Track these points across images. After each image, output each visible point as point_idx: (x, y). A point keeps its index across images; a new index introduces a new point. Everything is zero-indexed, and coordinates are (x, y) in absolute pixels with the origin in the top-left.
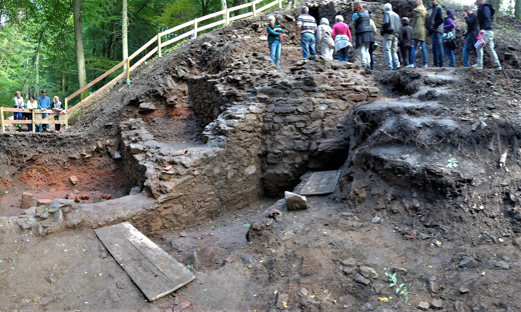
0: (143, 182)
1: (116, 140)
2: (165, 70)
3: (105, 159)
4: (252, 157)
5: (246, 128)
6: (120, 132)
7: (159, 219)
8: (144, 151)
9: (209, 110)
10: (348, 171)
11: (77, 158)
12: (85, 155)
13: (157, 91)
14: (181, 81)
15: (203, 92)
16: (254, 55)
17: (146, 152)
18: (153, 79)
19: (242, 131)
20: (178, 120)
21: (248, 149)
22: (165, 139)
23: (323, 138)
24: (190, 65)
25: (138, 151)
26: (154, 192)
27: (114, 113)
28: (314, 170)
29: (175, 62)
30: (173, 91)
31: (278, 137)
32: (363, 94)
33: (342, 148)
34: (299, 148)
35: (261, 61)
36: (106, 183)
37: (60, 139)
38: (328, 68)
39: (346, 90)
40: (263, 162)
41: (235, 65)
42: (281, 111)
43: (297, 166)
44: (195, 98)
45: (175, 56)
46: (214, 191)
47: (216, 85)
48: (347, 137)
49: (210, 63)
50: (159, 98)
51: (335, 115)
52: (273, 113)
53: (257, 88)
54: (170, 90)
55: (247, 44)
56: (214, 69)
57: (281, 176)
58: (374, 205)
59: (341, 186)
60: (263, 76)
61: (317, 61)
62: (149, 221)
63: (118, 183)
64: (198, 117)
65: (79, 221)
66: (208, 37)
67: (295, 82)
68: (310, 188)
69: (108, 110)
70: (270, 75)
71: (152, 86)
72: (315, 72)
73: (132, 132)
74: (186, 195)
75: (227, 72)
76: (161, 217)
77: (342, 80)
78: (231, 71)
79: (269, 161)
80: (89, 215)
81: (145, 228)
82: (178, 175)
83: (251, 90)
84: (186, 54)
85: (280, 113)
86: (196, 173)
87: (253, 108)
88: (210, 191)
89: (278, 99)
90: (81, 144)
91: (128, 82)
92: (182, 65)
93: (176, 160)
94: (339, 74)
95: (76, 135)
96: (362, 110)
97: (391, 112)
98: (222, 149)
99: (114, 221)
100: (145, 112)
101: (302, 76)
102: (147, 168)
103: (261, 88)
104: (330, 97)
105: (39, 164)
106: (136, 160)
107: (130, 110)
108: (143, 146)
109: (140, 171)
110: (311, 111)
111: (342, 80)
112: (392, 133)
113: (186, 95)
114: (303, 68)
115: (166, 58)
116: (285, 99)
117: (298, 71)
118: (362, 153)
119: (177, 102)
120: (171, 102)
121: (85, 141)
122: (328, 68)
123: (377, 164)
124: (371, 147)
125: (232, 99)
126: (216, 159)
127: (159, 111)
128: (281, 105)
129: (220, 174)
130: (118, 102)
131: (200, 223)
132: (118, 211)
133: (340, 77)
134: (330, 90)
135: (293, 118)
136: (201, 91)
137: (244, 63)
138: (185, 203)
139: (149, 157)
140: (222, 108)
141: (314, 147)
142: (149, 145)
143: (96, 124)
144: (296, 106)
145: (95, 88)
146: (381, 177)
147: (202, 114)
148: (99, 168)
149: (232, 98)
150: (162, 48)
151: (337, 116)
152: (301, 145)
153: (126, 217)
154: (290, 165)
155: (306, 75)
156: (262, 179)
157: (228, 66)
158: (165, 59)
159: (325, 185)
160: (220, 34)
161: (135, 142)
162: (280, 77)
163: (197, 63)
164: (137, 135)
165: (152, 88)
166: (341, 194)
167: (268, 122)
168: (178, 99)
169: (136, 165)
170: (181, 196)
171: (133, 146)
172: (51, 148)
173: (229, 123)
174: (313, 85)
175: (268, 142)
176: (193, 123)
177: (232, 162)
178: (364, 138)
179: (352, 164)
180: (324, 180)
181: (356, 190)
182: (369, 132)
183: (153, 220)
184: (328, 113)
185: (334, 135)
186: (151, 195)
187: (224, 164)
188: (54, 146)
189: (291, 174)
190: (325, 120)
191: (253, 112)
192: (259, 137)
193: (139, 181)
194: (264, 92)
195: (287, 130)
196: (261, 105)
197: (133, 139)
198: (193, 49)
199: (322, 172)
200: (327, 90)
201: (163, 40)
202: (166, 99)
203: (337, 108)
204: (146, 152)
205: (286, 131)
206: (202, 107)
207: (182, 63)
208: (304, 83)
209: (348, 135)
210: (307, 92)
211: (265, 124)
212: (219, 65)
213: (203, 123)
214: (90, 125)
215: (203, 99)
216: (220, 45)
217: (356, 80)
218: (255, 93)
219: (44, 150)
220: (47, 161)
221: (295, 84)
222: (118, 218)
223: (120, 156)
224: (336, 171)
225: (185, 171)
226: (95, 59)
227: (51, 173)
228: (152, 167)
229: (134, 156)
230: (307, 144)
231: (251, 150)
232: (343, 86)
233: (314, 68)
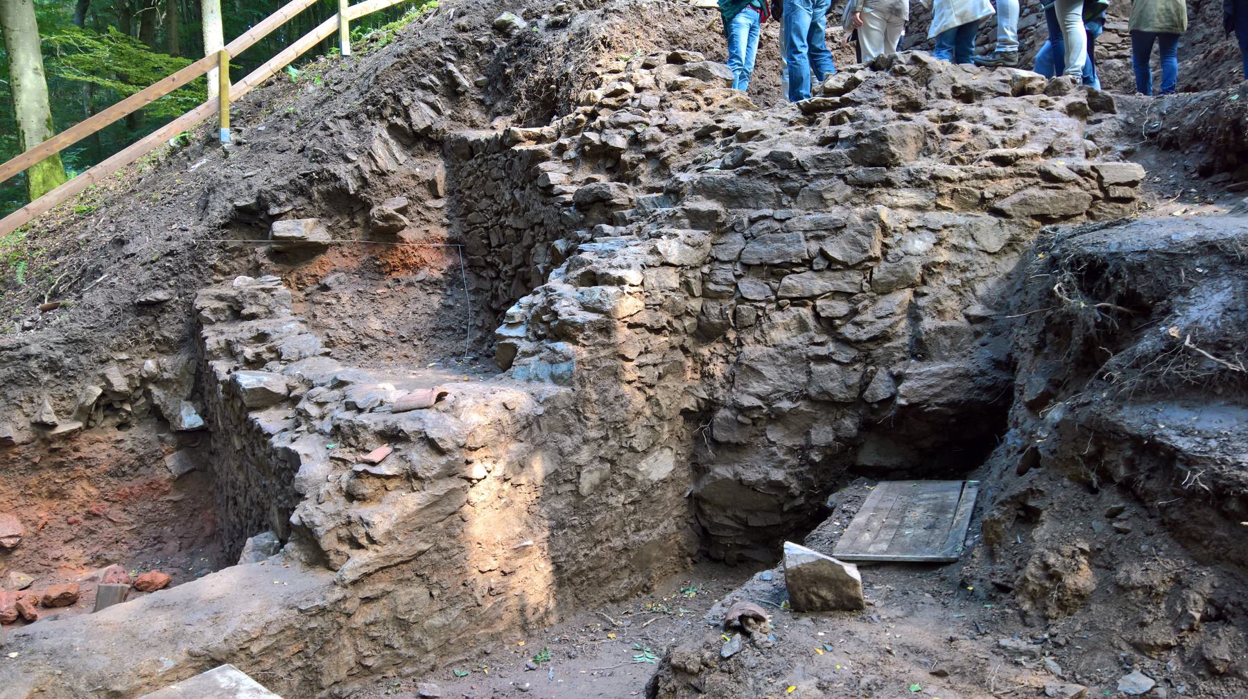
0: (287, 512)
1: (182, 358)
2: (366, 103)
3: (139, 435)
6: (200, 327)
7: (346, 640)
8: (290, 399)
9: (517, 253)
10: (1019, 486)
11: (17, 438)
12: (54, 426)
13: (335, 178)
14: (421, 146)
15: (497, 187)
16: (674, 59)
17: (297, 399)
18: (321, 134)
19: (630, 326)
20: (410, 284)
21: (651, 392)
22: (365, 354)
23: (914, 356)
24: (453, 91)
25: (267, 399)
26: (328, 543)
27: (171, 253)
28: (878, 474)
29: (400, 75)
30: (393, 180)
31: (752, 350)
32: (1077, 190)
33: (985, 397)
34: (826, 392)
35: (697, 82)
36: (150, 531)
38: (941, 96)
39: (1011, 176)
40: (697, 439)
41: (608, 96)
42: (766, 259)
44: (469, 210)
47: (542, 165)
48: (1003, 358)
49: (521, 86)
50: (344, 204)
51: (964, 270)
52: (738, 267)
53: (684, 177)
54: (383, 174)
55: (647, 23)
57: (761, 489)
58: (1125, 628)
59: (989, 536)
60: (704, 135)
61: (901, 72)
62: (310, 651)
63: (197, 524)
64: (479, 277)
67: (819, 151)
68: (867, 537)
69: (146, 244)
70: (727, 132)
71: (317, 157)
72: (895, 114)
73: (244, 330)
74: (439, 550)
75: (579, 121)
77: (996, 137)
78: (593, 116)
79: (721, 435)
80: (70, 661)
81: (297, 679)
82: (411, 478)
83: (663, 183)
85: (761, 265)
87: (672, 249)
89: (755, 214)
90: (34, 380)
92: (424, 87)
93: (407, 424)
94: (984, 118)
96: (1088, 250)
97: (1215, 259)
98: (563, 390)
99: (176, 669)
100: (293, 254)
101: (846, 130)
102: (303, 460)
103: (698, 176)
104: (946, 202)
106: (260, 430)
107: (233, 243)
108: (286, 379)
109: (277, 474)
110: (876, 259)
111: (996, 137)
112: (1220, 348)
113: (437, 197)
115: (370, 60)
116: (780, 214)
117: (828, 115)
118: (1083, 418)
119: (406, 220)
120: (387, 218)
121: (53, 366)
122: (941, 96)
123: (1143, 468)
124: (1119, 401)
125: (595, 214)
126: (543, 422)
127: (346, 250)
128: (767, 235)
130: (188, 212)
132: (190, 629)
133: (987, 129)
134: (948, 180)
136: (490, 183)
138: (435, 579)
139: (308, 417)
140: (560, 245)
141: (880, 388)
143: (95, 296)
144: (818, 238)
145: (91, 152)
146: (1163, 523)
147: (492, 265)
148: (117, 472)
149: (596, 208)
150: (353, 24)
151: (968, 275)
152: (832, 380)
153: (225, 647)
154: (791, 451)
155: (861, 126)
156: (695, 502)
157: (582, 98)
158: (365, 64)
159: (921, 531)
161: (257, 363)
162: (763, 137)
163: (476, 84)
164: (262, 337)
165: (316, 167)
166: (988, 568)
167: (717, 296)
168: (411, 210)
169: (260, 453)
170: (422, 553)
171: (248, 379)
173: (586, 298)
174: (887, 161)
175: (718, 369)
176: (464, 299)
178: (1089, 363)
179: (1032, 459)
180: (917, 514)
181: (1052, 560)
182: (1112, 337)
183: (328, 648)
185: (954, 347)
186: (319, 558)
187: (568, 443)
189: (794, 485)
190: (925, 289)
191: (671, 260)
192: (685, 351)
193: (274, 509)
194: (707, 189)
196: (698, 235)
197: (249, 352)
198: (465, 35)
199: (909, 485)
200: (935, 178)
202: (370, 207)
203: (970, 244)
204: (297, 399)
206: (494, 242)
207: (425, 80)
208: (852, 155)
209: (1008, 348)
210: (862, 187)
211: (710, 304)
212: (550, 96)
213: (495, 297)
214: (70, 301)
215: (498, 214)
217: (1050, 137)
218: (675, 194)
221: (819, 161)
222: (190, 653)
224: (959, 483)
225: (436, 463)
226: (88, 41)
228: (322, 453)
229: (253, 415)
230: (855, 379)
232: (1001, 161)
233: (889, 101)
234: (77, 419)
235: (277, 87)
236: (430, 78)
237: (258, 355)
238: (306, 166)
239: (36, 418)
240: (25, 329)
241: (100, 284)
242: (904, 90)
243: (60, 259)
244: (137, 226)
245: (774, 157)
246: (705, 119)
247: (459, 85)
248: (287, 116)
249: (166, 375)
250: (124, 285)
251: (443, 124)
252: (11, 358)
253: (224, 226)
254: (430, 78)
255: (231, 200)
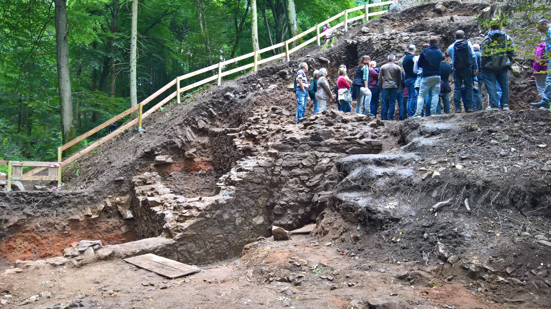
2: (185, 120)
4: (260, 207)
5: (255, 180)
6: (133, 187)
8: (162, 204)
11: (81, 220)
12: (91, 216)
13: (174, 143)
18: (171, 130)
19: (250, 182)
20: (196, 175)
24: (211, 116)
25: (156, 204)
27: (125, 166)
29: (195, 112)
35: (279, 116)
37: (58, 198)
43: (299, 217)
44: (215, 152)
45: (195, 106)
46: (223, 234)
47: (234, 140)
55: (268, 97)
56: (236, 122)
60: (278, 132)
64: (217, 173)
65: (110, 252)
66: (231, 86)
70: (284, 131)
71: (170, 137)
74: (198, 235)
76: (177, 252)
78: (250, 125)
79: (276, 212)
84: (208, 104)
86: (208, 216)
88: (219, 234)
89: (286, 153)
90: (85, 203)
91: (140, 130)
92: (202, 115)
95: (77, 191)
100: (161, 167)
105: (28, 231)
107: (143, 163)
114: (314, 123)
115: (186, 106)
116: (292, 153)
117: (309, 127)
120: (190, 155)
121: (91, 199)
122: (339, 122)
124: (338, 192)
125: (247, 154)
126: (226, 206)
127: (177, 165)
129: (228, 220)
130: (130, 154)
131: (211, 262)
135: (297, 171)
136: (221, 144)
137: (263, 118)
139: (167, 206)
142: (166, 197)
147: (221, 169)
152: (303, 196)
154: (293, 216)
160: (244, 83)
161: (152, 195)
164: (153, 189)
165: (169, 140)
167: (277, 175)
171: (150, 199)
172: (45, 210)
177: (240, 210)
184: (329, 166)
187: (233, 212)
188: (50, 206)
190: (326, 173)
192: (267, 189)
195: (292, 183)
196: (270, 159)
198: (216, 100)
201: (183, 83)
202: (185, 152)
205: (292, 184)
206: (222, 162)
214: (94, 180)
215: (223, 153)
216: (242, 98)
219: (35, 213)
220: (39, 226)
221: (303, 140)
223: (132, 216)
227: (44, 241)
231: (259, 201)
234: (97, 214)
235: (156, 113)
236: (204, 113)
237: (152, 194)
238: (166, 140)
239: (86, 214)
240: (81, 189)
241: (104, 175)
242: (329, 120)
243: (90, 168)
244: (115, 158)
245: (292, 139)
246: (279, 126)
247: (213, 114)
248: (160, 124)
249: (122, 202)
250: (111, 175)
251: (208, 126)
252: (80, 196)
253: (141, 158)
254: (204, 113)
255: (143, 150)
